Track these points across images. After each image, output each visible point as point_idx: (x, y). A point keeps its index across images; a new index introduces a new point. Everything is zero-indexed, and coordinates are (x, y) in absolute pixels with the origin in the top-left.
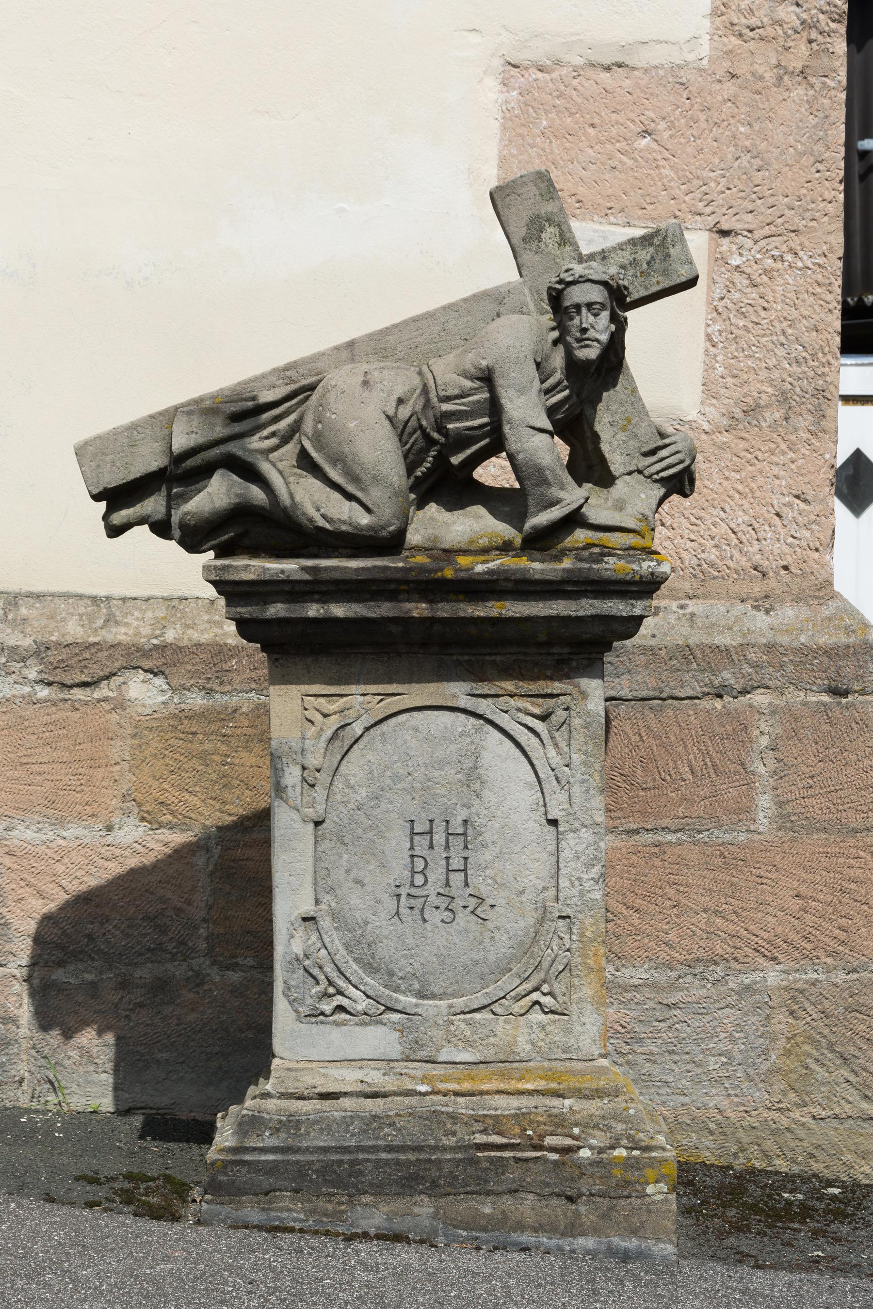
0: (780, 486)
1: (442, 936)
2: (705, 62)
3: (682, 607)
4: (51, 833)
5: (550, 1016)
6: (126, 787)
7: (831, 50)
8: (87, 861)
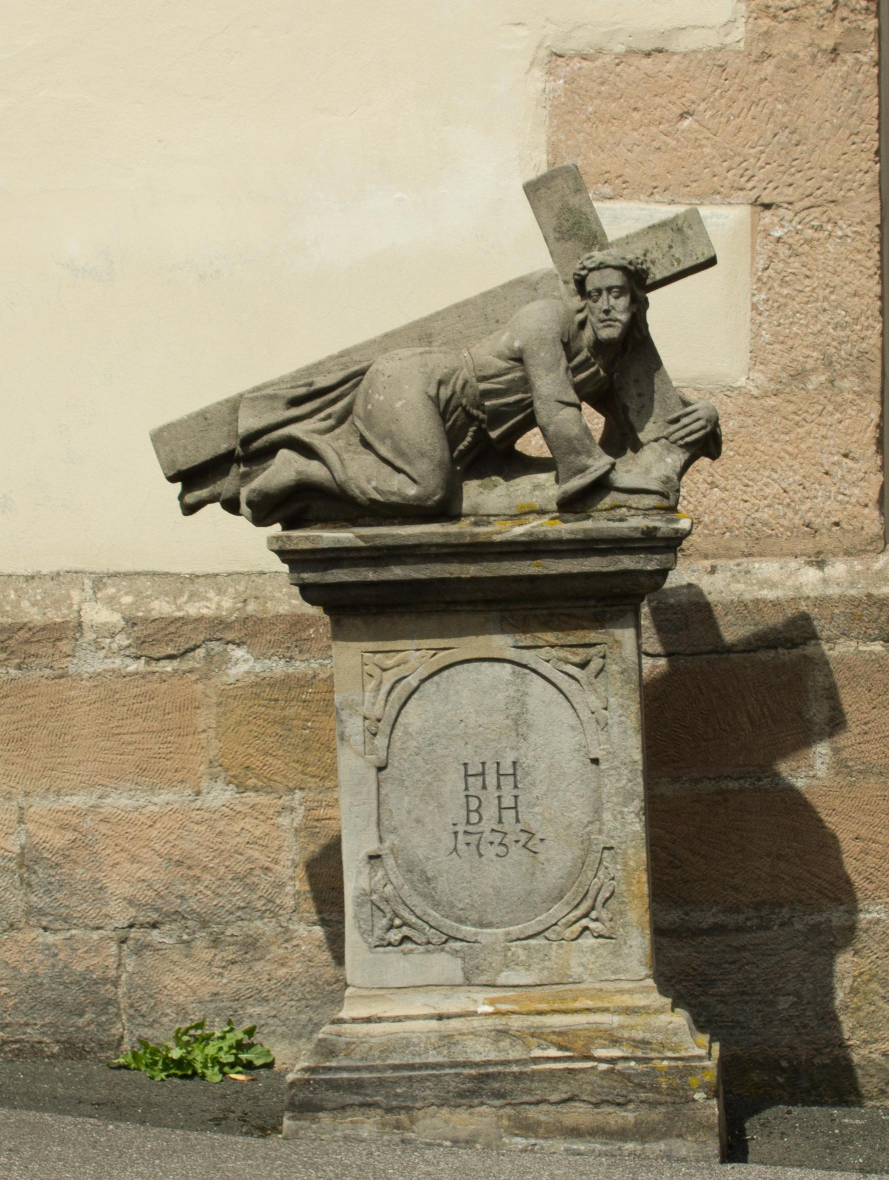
0: (829, 446)
1: (497, 869)
2: (742, 44)
3: (738, 565)
4: (143, 800)
5: (601, 940)
6: (213, 753)
7: (862, 27)
8: (178, 826)
